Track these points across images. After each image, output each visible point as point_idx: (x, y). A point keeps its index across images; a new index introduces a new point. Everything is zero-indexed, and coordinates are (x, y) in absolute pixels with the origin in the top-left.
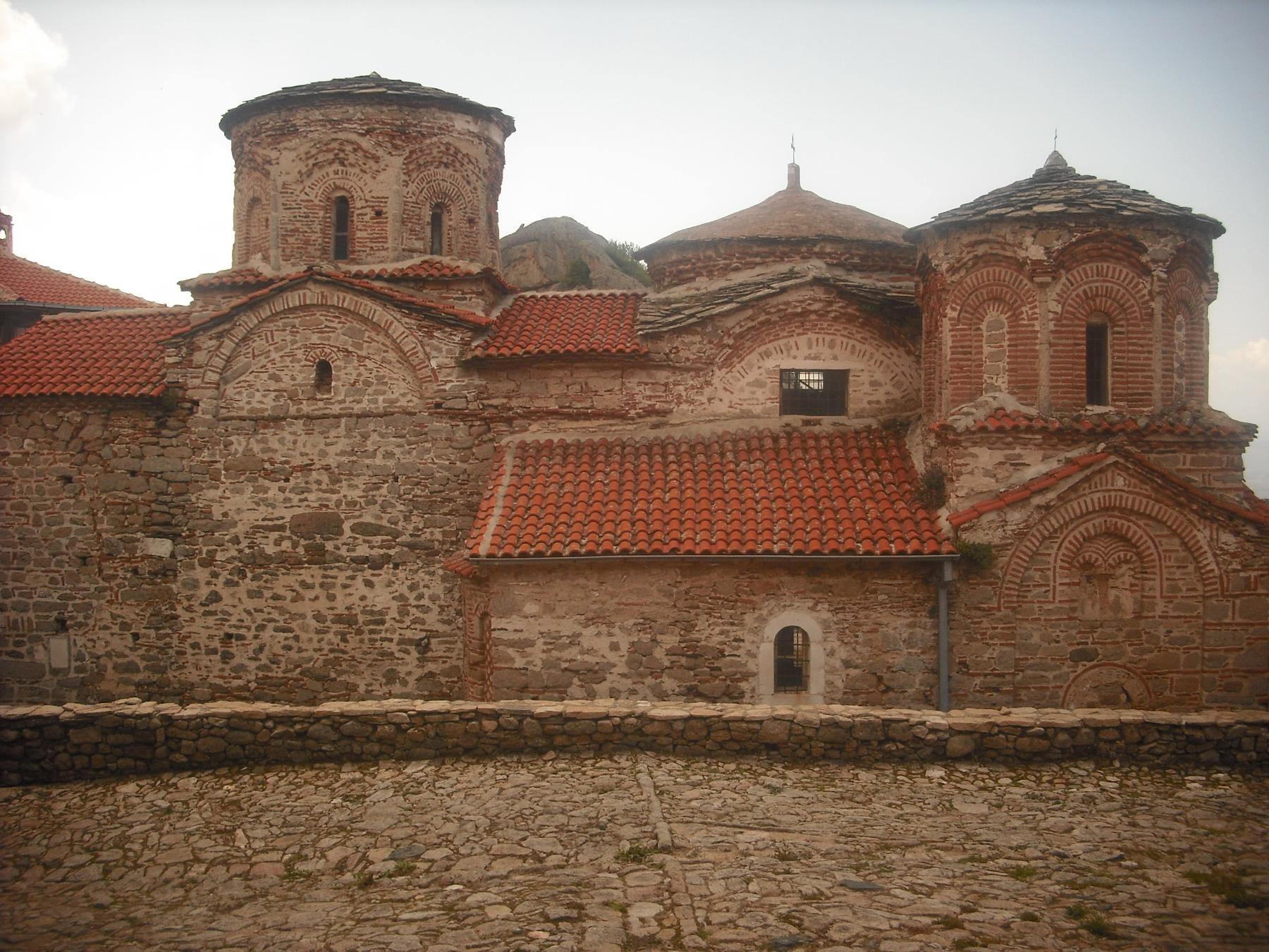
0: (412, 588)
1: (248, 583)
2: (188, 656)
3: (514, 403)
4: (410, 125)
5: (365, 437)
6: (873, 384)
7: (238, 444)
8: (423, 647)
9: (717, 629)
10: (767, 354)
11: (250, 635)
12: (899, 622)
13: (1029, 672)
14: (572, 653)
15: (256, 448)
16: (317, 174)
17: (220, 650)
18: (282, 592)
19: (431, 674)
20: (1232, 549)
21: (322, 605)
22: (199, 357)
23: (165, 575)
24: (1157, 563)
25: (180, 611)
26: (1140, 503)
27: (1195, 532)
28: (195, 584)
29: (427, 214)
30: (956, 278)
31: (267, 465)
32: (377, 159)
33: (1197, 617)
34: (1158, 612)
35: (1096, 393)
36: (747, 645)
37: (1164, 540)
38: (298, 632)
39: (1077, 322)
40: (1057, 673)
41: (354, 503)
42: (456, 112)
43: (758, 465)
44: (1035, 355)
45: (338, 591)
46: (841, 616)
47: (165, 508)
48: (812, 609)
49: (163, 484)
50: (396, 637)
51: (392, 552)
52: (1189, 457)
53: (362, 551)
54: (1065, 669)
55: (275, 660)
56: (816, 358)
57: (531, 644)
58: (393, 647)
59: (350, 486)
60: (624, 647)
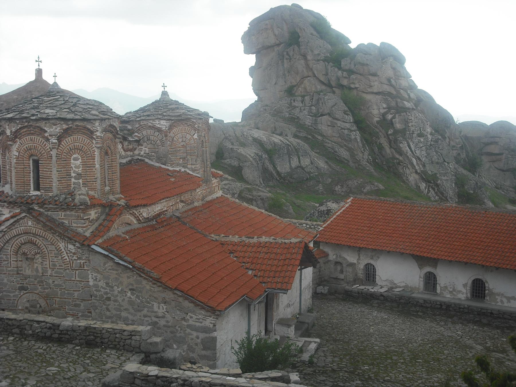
13: (4, 293)
20: (73, 251)
24: (47, 255)
27: (59, 244)
33: (63, 277)
34: (49, 274)
37: (49, 246)
39: (25, 159)
40: (14, 294)
52: (63, 213)
54: (17, 293)
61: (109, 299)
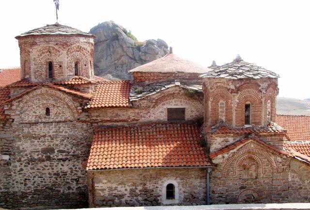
0: (74, 166)
1: (30, 166)
2: (15, 185)
3: (98, 118)
4: (68, 42)
5: (60, 128)
6: (191, 111)
7: (26, 130)
8: (77, 181)
9: (152, 185)
10: (164, 104)
11: (32, 179)
12: (197, 182)
14: (115, 192)
15: (31, 131)
16: (43, 55)
17: (24, 183)
18: (39, 168)
19: (80, 187)
21: (50, 171)
22: (14, 107)
23: (8, 164)
25: (12, 173)
26: (257, 151)
28: (16, 167)
29: (73, 65)
30: (212, 91)
31: (34, 136)
32: (59, 51)
34: (261, 177)
35: (247, 122)
36: (159, 189)
38: (44, 178)
41: (57, 145)
42: (80, 37)
43: (162, 136)
44: (232, 113)
45: (54, 167)
46: (183, 181)
47: (7, 147)
48: (176, 179)
49: (6, 141)
50: (70, 178)
51: (68, 157)
52: (270, 138)
53: (60, 157)
55: (38, 185)
56: (177, 105)
57: (105, 190)
58: (69, 181)
59: (56, 140)
60: (129, 190)
61: (301, 188)
